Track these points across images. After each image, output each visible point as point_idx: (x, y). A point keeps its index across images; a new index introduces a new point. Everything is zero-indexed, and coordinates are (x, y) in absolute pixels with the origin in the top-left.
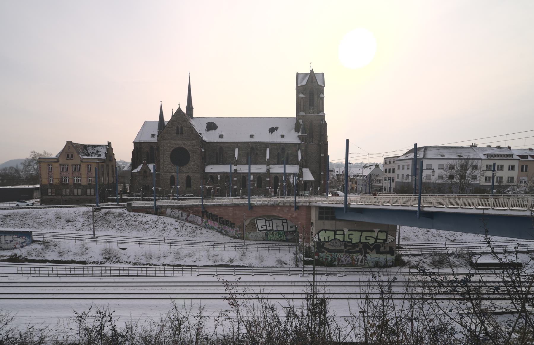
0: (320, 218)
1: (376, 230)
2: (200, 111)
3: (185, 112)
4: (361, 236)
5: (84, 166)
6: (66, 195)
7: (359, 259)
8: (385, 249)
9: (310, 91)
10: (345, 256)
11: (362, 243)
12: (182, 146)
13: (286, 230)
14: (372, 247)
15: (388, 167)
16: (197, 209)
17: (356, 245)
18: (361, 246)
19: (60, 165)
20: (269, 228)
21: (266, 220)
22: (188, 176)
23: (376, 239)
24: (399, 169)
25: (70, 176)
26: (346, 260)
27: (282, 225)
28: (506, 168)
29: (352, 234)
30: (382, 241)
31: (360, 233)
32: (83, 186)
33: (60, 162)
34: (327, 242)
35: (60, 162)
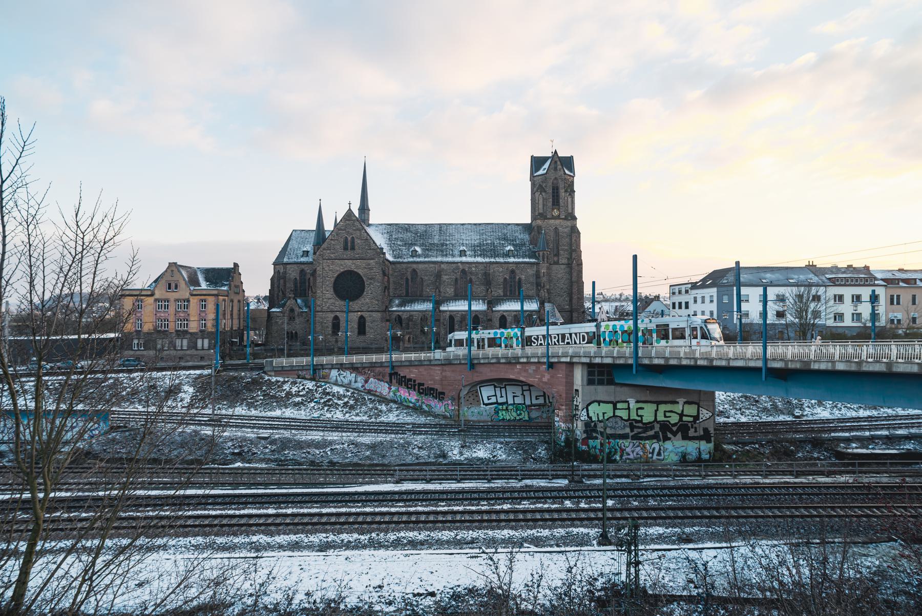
0: (590, 382)
1: (681, 401)
2: (382, 214)
3: (357, 215)
4: (656, 411)
5: (194, 301)
6: (203, 349)
7: (654, 449)
8: (696, 431)
9: (553, 181)
10: (631, 445)
11: (658, 422)
12: (353, 268)
13: (528, 402)
14: (675, 429)
15: (677, 299)
16: (381, 369)
17: (648, 426)
18: (657, 427)
19: (156, 300)
20: (500, 400)
21: (495, 387)
22: (362, 317)
23: (681, 415)
24: (695, 301)
25: (171, 318)
26: (633, 452)
27: (522, 394)
28: (848, 299)
29: (642, 408)
30: (691, 419)
31: (654, 406)
32: (191, 334)
33: (157, 296)
34: (601, 422)
35: (157, 296)
